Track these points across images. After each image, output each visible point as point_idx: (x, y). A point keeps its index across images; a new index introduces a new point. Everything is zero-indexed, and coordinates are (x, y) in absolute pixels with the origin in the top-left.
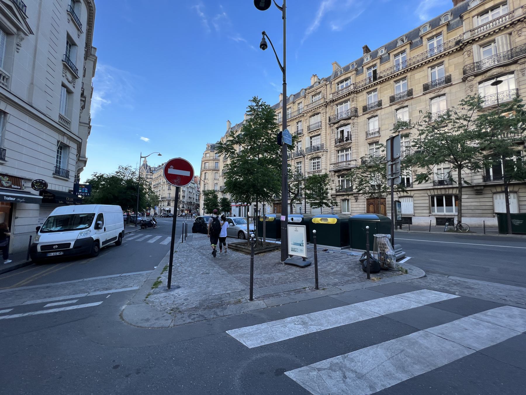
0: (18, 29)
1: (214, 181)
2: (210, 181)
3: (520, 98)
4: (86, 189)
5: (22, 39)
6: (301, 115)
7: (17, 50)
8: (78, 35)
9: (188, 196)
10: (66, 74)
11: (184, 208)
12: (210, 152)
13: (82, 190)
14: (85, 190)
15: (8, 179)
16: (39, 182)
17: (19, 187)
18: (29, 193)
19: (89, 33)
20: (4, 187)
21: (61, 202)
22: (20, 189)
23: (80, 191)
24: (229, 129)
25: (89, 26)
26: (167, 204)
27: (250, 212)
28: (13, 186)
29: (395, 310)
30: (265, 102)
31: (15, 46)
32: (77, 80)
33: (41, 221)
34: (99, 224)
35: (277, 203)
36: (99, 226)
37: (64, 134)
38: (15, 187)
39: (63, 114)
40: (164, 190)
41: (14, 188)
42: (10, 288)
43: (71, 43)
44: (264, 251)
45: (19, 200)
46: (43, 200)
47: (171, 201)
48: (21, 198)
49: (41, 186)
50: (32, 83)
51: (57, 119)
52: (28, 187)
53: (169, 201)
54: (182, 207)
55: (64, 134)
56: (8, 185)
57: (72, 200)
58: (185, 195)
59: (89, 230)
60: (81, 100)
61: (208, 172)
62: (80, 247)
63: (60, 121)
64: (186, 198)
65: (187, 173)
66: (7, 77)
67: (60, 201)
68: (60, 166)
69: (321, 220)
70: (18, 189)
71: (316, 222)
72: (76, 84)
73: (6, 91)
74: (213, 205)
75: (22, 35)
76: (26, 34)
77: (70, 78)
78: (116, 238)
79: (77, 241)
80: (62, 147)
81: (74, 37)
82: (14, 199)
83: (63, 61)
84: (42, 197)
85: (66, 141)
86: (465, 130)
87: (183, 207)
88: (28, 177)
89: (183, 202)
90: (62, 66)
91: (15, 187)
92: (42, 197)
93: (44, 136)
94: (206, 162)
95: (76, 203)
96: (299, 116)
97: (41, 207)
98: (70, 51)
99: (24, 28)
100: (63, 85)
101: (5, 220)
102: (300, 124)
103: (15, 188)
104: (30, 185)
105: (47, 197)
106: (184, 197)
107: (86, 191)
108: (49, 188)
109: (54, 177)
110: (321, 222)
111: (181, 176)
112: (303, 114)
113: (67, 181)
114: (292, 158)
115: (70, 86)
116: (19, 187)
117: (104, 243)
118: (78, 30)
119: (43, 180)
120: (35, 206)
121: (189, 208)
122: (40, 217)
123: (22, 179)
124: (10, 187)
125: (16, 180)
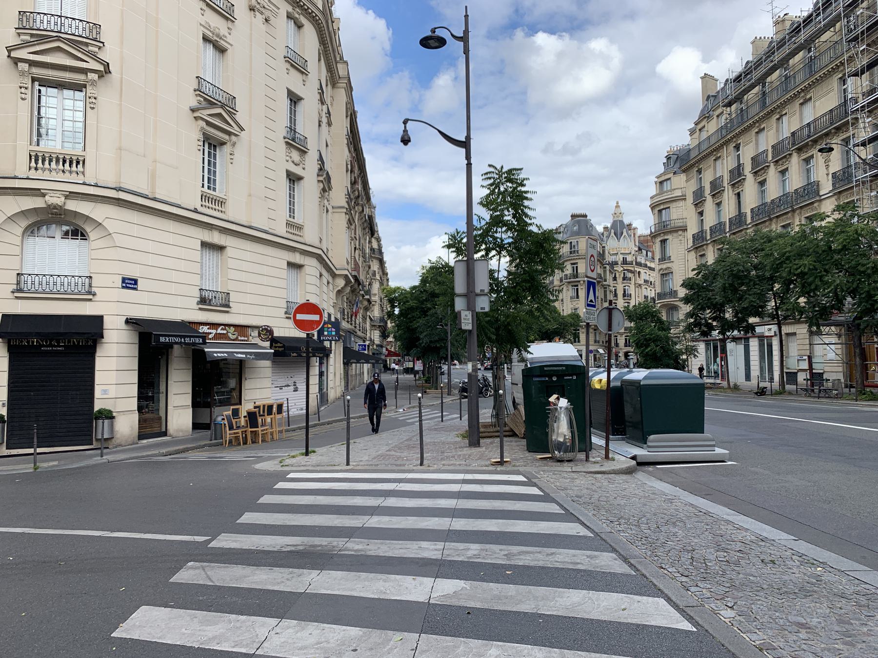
0: (229, 134)
3: (499, 167)
4: (333, 330)
5: (234, 144)
7: (231, 161)
8: (303, 81)
10: (290, 155)
12: (671, 175)
13: (328, 331)
14: (332, 331)
15: (234, 329)
16: (266, 329)
17: (246, 339)
18: (255, 346)
19: (327, 56)
20: (231, 340)
21: (295, 354)
23: (326, 333)
25: (324, 45)
28: (240, 338)
29: (536, 563)
33: (276, 383)
38: (243, 338)
40: (562, 300)
41: (241, 340)
43: (294, 99)
45: (248, 356)
46: (276, 354)
48: (250, 353)
49: (267, 335)
52: (254, 338)
56: (235, 337)
60: (319, 181)
61: (669, 237)
63: (288, 230)
65: (300, 317)
66: (224, 201)
67: (293, 353)
70: (245, 340)
72: (306, 163)
73: (218, 220)
77: (295, 156)
81: (298, 91)
82: (244, 356)
84: (273, 351)
86: (483, 230)
88: (254, 323)
90: (284, 146)
91: (243, 338)
92: (273, 351)
94: (662, 207)
95: (317, 354)
97: (273, 362)
98: (295, 111)
103: (243, 340)
107: (334, 333)
108: (276, 334)
113: (227, 312)
116: (246, 339)
119: (268, 326)
120: (267, 363)
122: (273, 377)
123: (248, 327)
125: (242, 329)
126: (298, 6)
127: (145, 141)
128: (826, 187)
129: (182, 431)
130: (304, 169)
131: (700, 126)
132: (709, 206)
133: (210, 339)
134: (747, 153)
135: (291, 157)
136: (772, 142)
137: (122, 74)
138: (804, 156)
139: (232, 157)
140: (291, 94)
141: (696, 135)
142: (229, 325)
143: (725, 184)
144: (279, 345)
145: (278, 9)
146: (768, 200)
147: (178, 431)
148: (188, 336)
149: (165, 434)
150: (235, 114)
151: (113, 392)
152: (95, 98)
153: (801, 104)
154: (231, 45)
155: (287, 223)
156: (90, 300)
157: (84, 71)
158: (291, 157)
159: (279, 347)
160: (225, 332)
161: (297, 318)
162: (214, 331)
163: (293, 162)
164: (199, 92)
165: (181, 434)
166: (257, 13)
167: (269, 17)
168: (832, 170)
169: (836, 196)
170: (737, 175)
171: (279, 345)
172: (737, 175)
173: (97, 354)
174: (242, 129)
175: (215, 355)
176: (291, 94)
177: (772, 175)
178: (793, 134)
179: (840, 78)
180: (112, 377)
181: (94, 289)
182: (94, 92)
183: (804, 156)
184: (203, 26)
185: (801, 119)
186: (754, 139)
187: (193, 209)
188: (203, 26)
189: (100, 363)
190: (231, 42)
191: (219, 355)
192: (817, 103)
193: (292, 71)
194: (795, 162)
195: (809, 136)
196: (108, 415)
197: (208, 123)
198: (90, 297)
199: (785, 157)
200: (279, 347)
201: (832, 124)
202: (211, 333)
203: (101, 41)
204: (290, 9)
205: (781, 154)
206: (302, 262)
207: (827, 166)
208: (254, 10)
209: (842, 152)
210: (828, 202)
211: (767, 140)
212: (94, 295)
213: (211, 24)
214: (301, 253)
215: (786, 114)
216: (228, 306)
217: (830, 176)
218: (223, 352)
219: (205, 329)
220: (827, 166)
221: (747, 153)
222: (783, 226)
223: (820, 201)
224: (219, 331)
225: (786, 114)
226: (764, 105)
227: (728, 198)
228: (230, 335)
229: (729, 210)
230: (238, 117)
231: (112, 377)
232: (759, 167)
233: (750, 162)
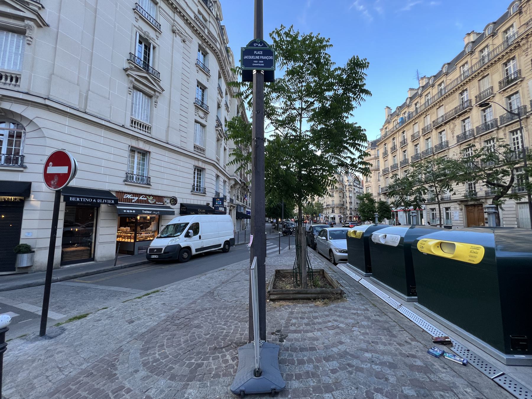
0: (155, 91)
1: (378, 183)
2: (373, 183)
5: (157, 97)
6: (512, 47)
9: (356, 202)
11: (352, 214)
12: (370, 150)
17: (162, 204)
18: (169, 207)
20: (151, 204)
22: (163, 204)
23: (217, 203)
24: (388, 116)
26: (331, 211)
27: (425, 219)
30: (319, 34)
31: (154, 103)
32: (208, 115)
34: (189, 232)
35: (472, 205)
36: (190, 234)
37: (198, 160)
39: (198, 144)
42: (93, 283)
44: (291, 296)
47: (335, 208)
50: (169, 127)
51: (192, 149)
53: (333, 208)
54: (350, 214)
55: (198, 160)
57: (204, 211)
58: (353, 201)
59: (178, 238)
62: (168, 252)
64: (353, 204)
68: (200, 185)
69: (441, 245)
71: (425, 251)
72: (208, 118)
74: (370, 211)
75: (157, 94)
76: (160, 93)
77: (201, 114)
78: (220, 245)
79: (168, 247)
80: (199, 170)
81: (204, 82)
83: (194, 103)
85: (201, 165)
87: (351, 214)
89: (351, 208)
90: (194, 107)
93: (182, 164)
96: (508, 50)
99: (158, 89)
100: (196, 122)
101: (156, 229)
102: (511, 64)
104: (168, 201)
105: (131, 211)
106: (351, 203)
107: (221, 203)
109: (192, 194)
110: (439, 253)
111: (58, 175)
112: (518, 42)
113: (205, 196)
114: (497, 126)
115: (203, 121)
116: (162, 204)
117: (197, 250)
118: (207, 75)
121: (357, 214)
123: (164, 197)
124: (155, 203)
125: (159, 198)
126: (205, 42)
127: (78, 76)
128: (453, 142)
129: (105, 258)
130: (206, 121)
131: (385, 127)
132: (390, 157)
133: (133, 202)
134: (408, 135)
135: (198, 114)
136: (422, 127)
137: (58, 29)
138: (426, 138)
139: (156, 104)
140: (199, 84)
141: (384, 130)
142: (149, 196)
143: (398, 148)
144: (184, 208)
145: (192, 39)
146: (419, 152)
147: (101, 258)
148: (109, 199)
149: (93, 259)
150: (159, 82)
151: (35, 234)
152: (31, 38)
153: (437, 109)
154: (159, 46)
155: (194, 146)
156: (22, 171)
157: (22, 19)
158: (198, 114)
159: (184, 209)
160: (145, 199)
161: (67, 167)
162: (137, 198)
163: (199, 116)
164: (130, 61)
165: (105, 259)
166: (177, 35)
167: (185, 39)
168: (456, 134)
169: (459, 146)
170: (404, 143)
171: (184, 208)
172: (404, 143)
173: (25, 208)
174: (163, 90)
175: (125, 211)
176: (199, 84)
177: (422, 141)
178: (434, 122)
179: (460, 93)
180: (36, 224)
181: (24, 164)
182: (31, 34)
183: (439, 130)
184: (136, 27)
185: (437, 115)
186: (412, 128)
187: (121, 125)
188: (136, 27)
189: (26, 215)
190: (158, 44)
191: (128, 211)
192: (447, 107)
193: (200, 71)
194: (434, 134)
195: (443, 121)
196: (28, 249)
197: (136, 80)
198: (21, 169)
199: (429, 132)
200: (184, 209)
201: (456, 114)
202: (134, 199)
203: (40, 3)
204: (200, 43)
205: (426, 132)
206: (203, 167)
207: (453, 133)
208: (175, 33)
209: (482, 116)
210: (453, 149)
211: (418, 128)
212: (25, 167)
213: (143, 28)
214: (202, 162)
215: (443, 105)
216: (150, 185)
217: (455, 138)
218: (132, 210)
219: (129, 196)
220: (453, 133)
221: (408, 135)
222: (486, 141)
223: (449, 149)
224: (141, 198)
225: (443, 105)
226: (417, 113)
227: (390, 157)
228: (149, 201)
229: (400, 157)
230: (161, 84)
231: (36, 224)
232: (415, 138)
233: (410, 137)
